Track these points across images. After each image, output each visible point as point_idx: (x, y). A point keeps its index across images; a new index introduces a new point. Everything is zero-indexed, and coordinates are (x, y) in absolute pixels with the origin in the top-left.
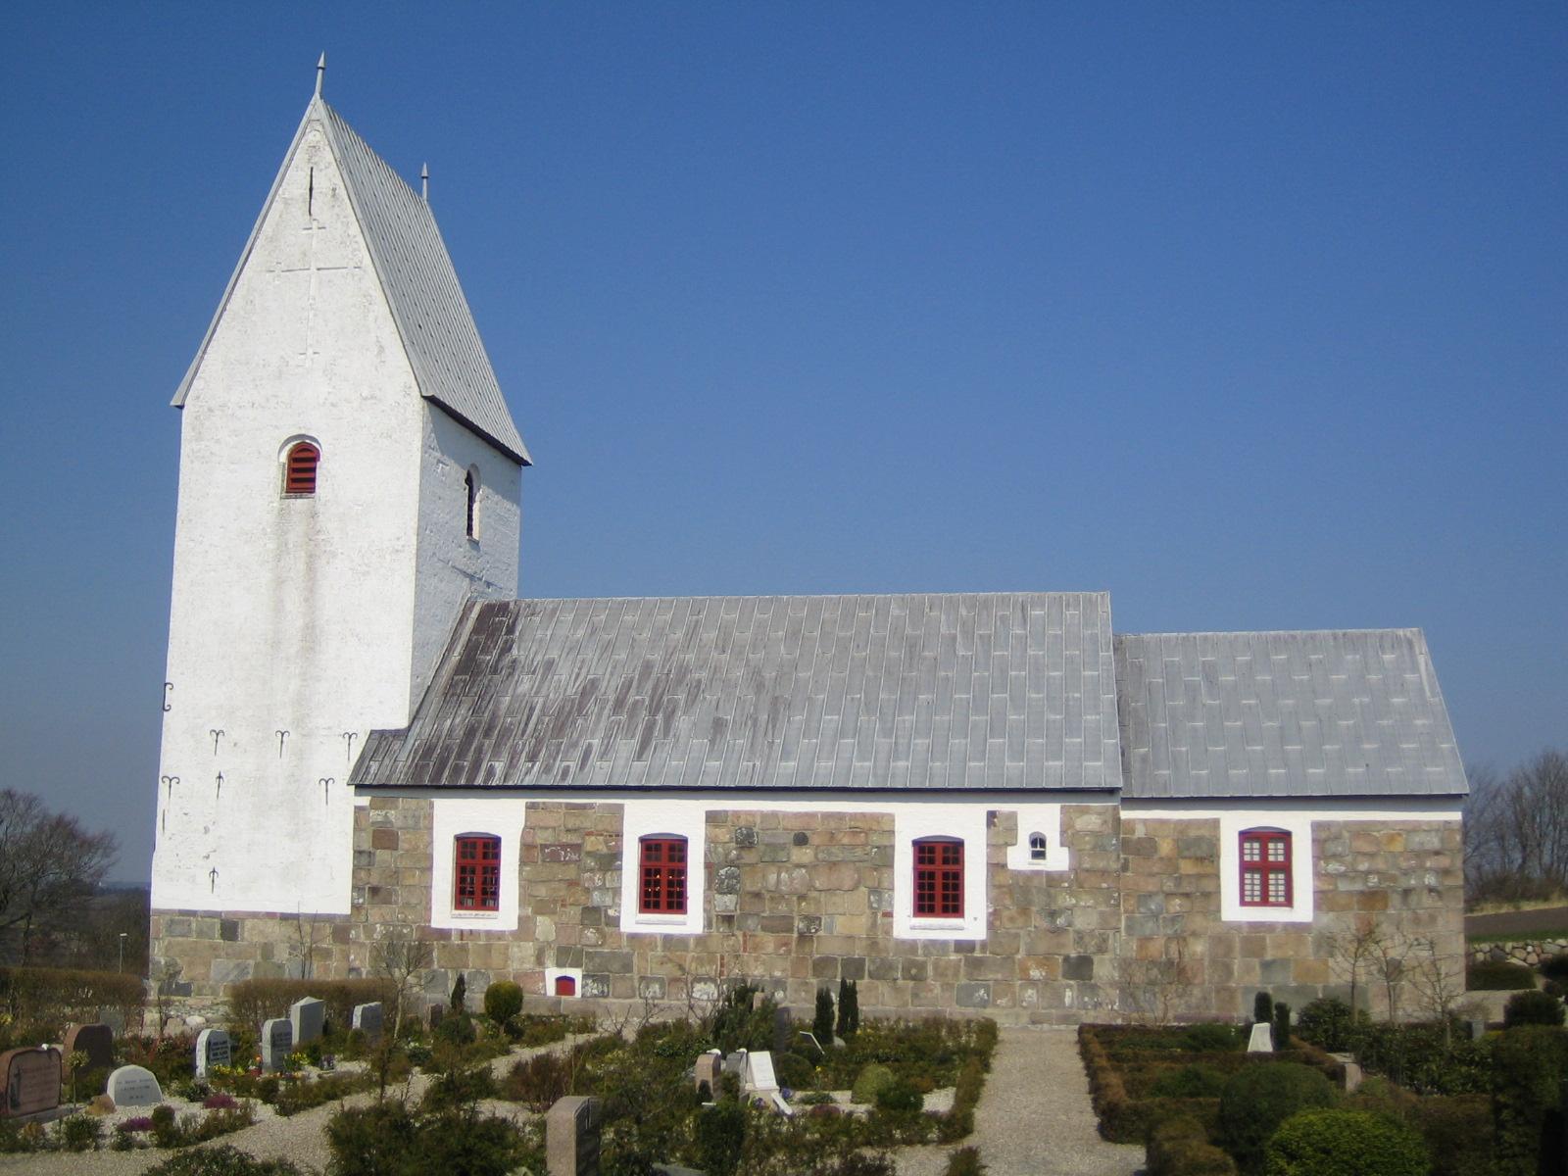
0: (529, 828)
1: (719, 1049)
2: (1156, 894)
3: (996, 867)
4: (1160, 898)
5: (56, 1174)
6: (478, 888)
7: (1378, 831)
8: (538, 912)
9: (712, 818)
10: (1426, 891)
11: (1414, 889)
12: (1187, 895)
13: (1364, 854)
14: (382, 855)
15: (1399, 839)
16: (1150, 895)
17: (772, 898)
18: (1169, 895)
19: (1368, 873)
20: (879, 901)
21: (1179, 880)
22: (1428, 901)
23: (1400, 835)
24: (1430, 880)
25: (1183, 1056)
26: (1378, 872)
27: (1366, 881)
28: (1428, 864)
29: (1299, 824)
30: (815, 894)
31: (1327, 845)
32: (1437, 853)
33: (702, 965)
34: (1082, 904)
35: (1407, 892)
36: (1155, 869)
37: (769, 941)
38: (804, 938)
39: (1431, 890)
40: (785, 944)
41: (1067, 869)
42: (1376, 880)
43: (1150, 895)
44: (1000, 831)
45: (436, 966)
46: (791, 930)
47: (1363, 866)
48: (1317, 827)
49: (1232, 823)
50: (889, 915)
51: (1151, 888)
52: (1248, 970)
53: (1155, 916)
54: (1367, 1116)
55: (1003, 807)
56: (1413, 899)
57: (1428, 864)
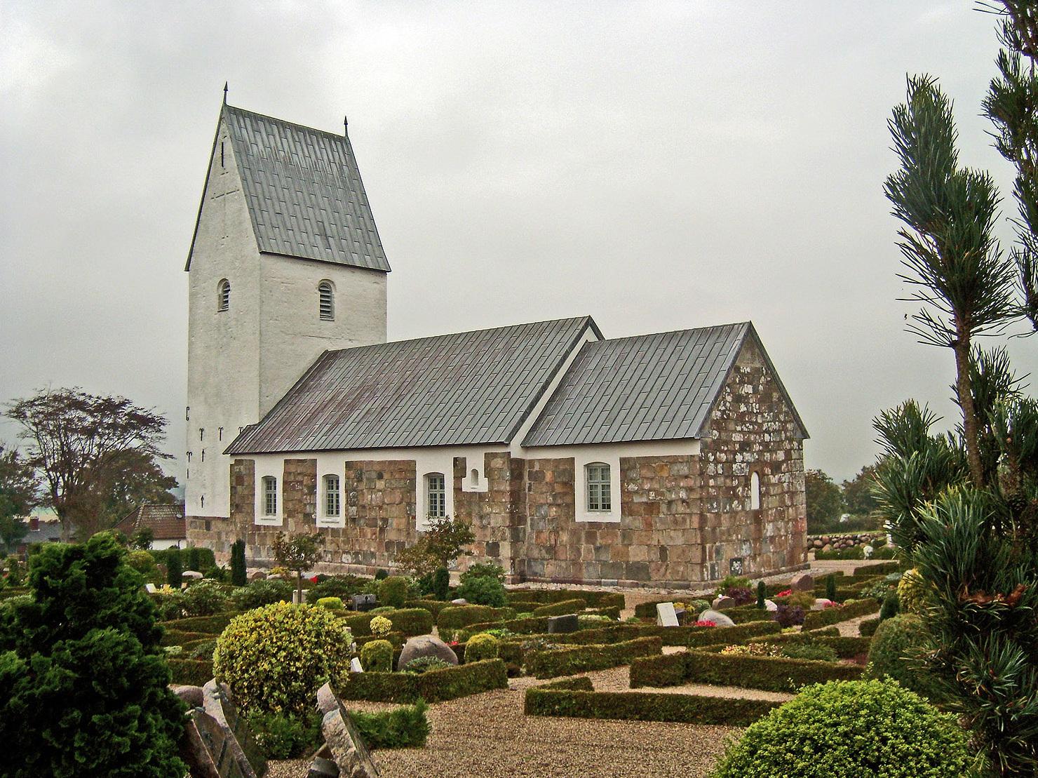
0: (287, 473)
1: (46, 625)
2: (545, 504)
3: (458, 490)
4: (546, 507)
5: (1034, 522)
6: (600, 503)
7: (655, 463)
8: (288, 517)
9: (349, 465)
10: (680, 502)
11: (674, 501)
12: (559, 505)
13: (647, 478)
14: (239, 488)
15: (666, 468)
16: (542, 505)
17: (370, 508)
18: (550, 505)
19: (650, 490)
20: (410, 510)
21: (554, 497)
22: (681, 508)
23: (666, 465)
24: (683, 495)
25: (581, 607)
26: (654, 490)
27: (648, 495)
28: (682, 484)
29: (612, 459)
30: (385, 506)
31: (628, 473)
32: (686, 477)
33: (345, 545)
34: (494, 511)
35: (670, 503)
36: (544, 490)
37: (368, 531)
38: (382, 530)
39: (683, 501)
40: (375, 534)
41: (487, 491)
42: (654, 495)
43: (542, 505)
44: (460, 468)
45: (257, 544)
46: (376, 526)
47: (646, 487)
48: (623, 461)
49: (582, 459)
50: (414, 518)
51: (542, 501)
52: (589, 551)
53: (544, 518)
54: (900, 592)
55: (460, 454)
56: (674, 507)
57: (682, 484)
